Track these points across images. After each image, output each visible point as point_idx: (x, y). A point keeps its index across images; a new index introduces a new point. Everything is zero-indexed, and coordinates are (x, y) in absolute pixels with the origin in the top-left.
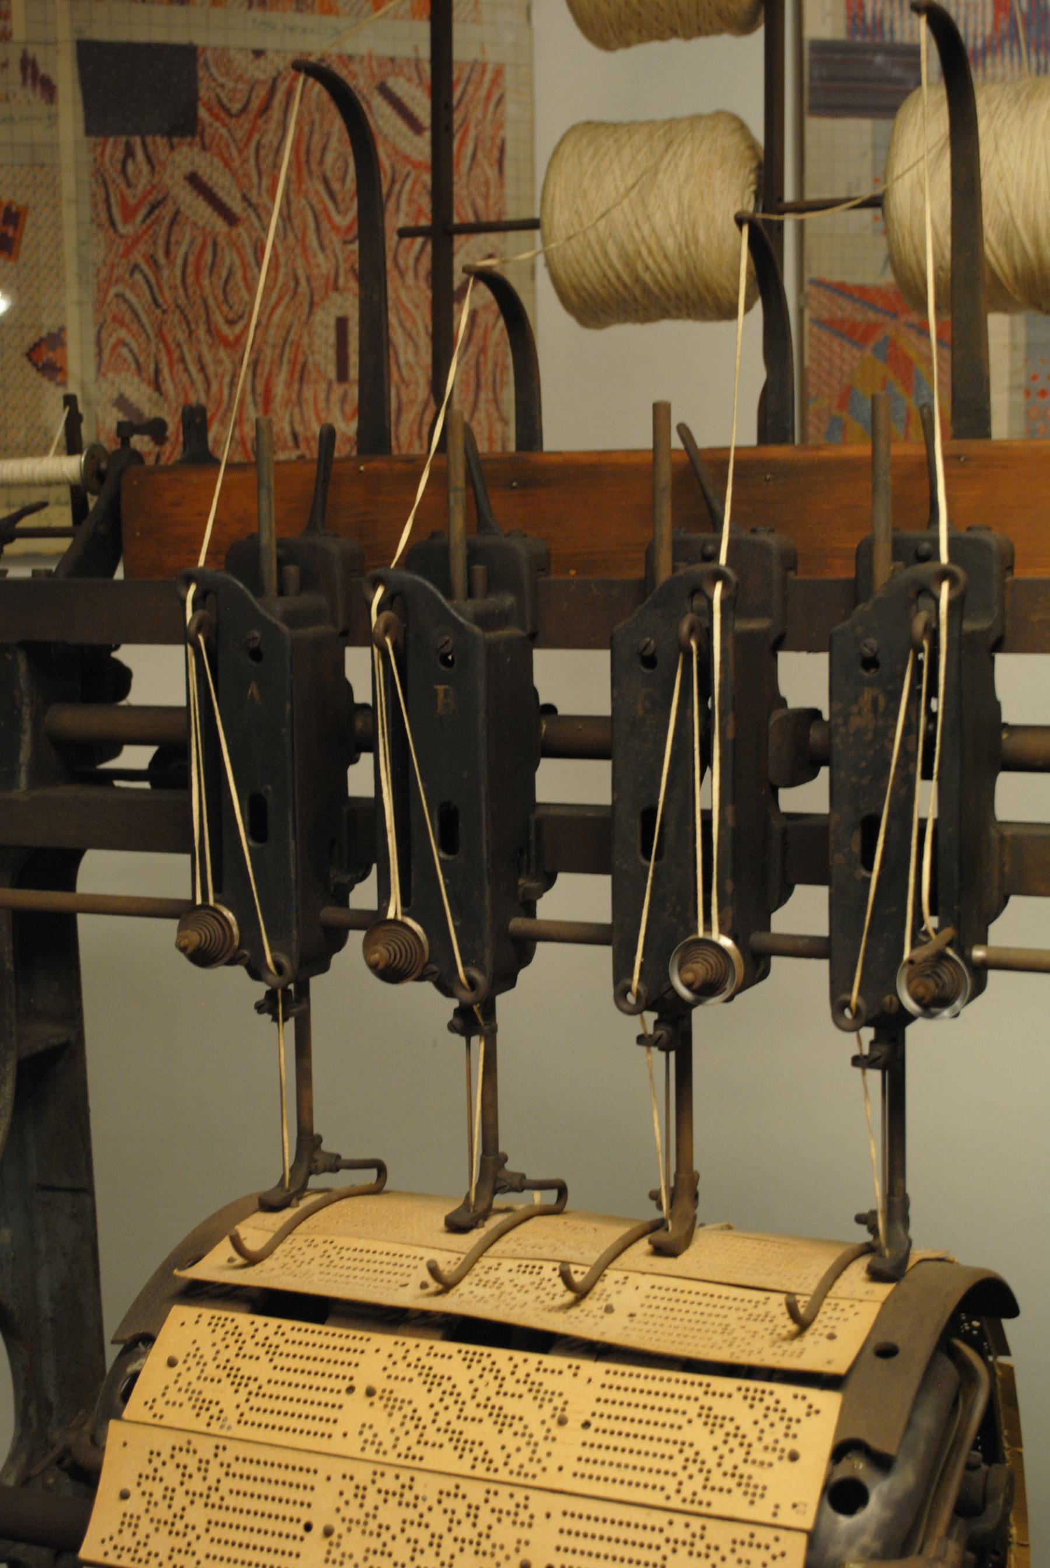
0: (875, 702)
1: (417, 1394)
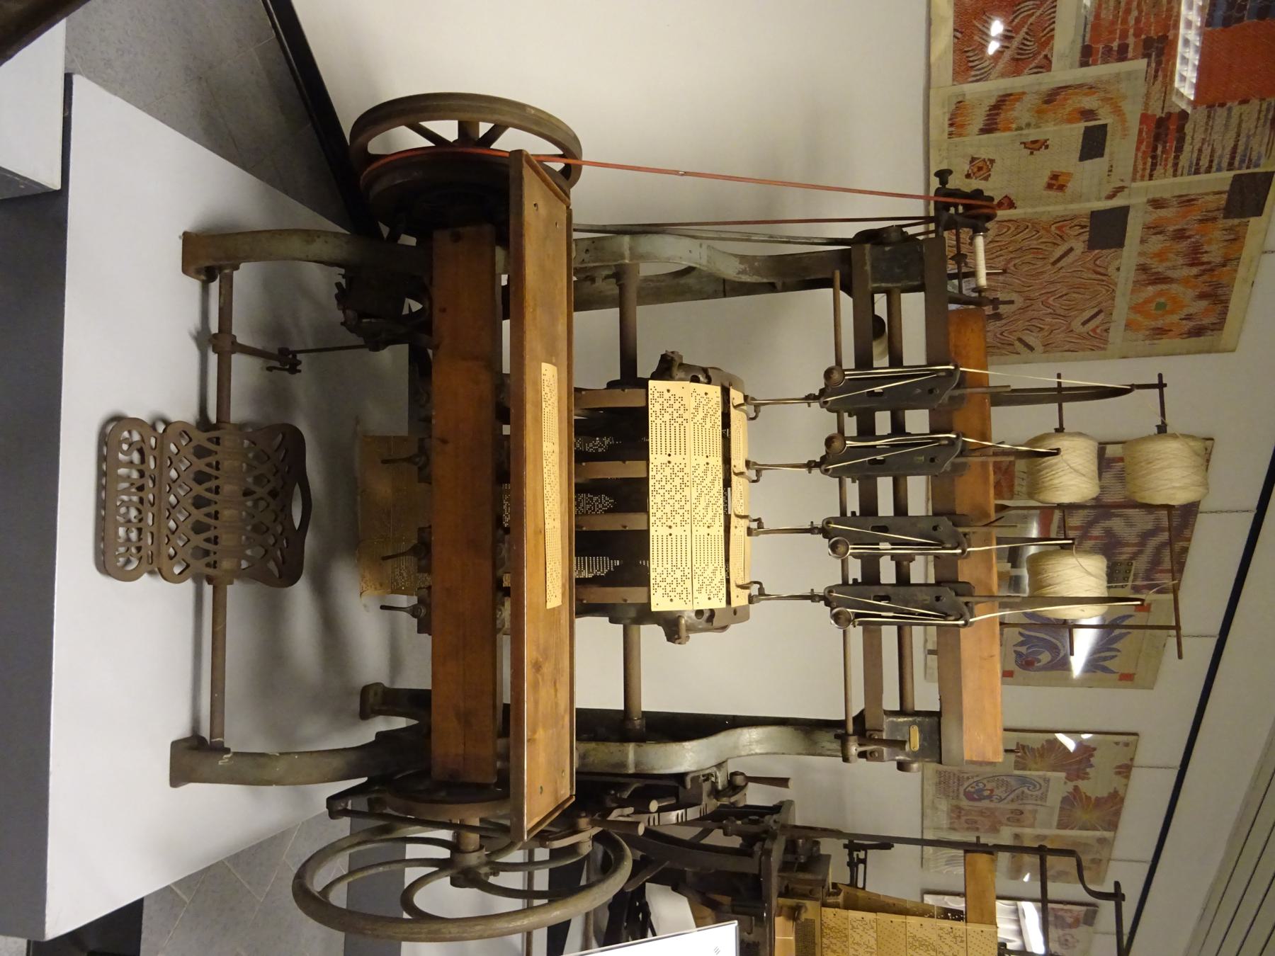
0: (926, 600)
1: (710, 478)
